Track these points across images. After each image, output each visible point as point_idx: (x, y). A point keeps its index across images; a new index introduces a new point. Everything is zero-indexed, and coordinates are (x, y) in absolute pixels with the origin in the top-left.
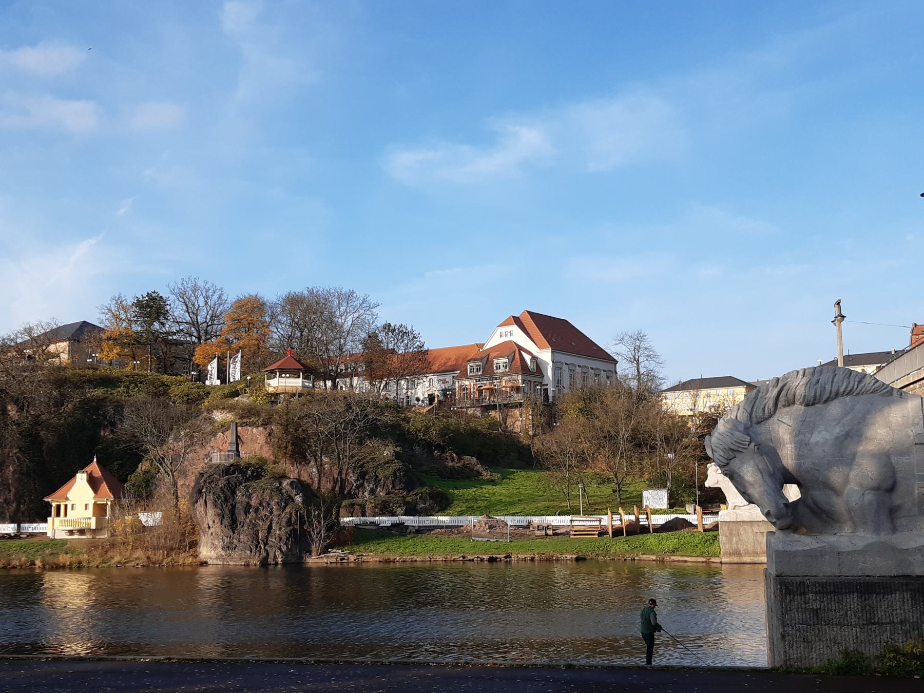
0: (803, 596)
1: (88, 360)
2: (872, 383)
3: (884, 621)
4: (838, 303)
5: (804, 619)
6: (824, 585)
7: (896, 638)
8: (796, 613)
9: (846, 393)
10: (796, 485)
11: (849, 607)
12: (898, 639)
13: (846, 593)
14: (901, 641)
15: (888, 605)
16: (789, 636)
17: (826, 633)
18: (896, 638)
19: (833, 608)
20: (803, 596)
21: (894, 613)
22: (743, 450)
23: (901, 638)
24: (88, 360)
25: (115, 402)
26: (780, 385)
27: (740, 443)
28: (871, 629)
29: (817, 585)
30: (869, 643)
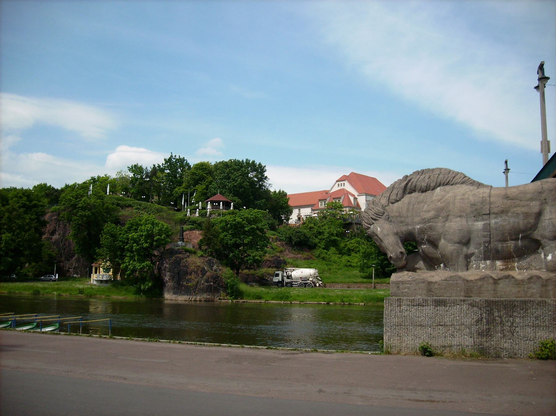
0: (399, 308)
1: (171, 203)
2: (462, 178)
3: (448, 324)
4: (506, 162)
5: (399, 322)
6: (413, 301)
7: (455, 335)
8: (394, 318)
9: (445, 184)
10: (59, 188)
11: (427, 315)
12: (456, 335)
13: (426, 306)
14: (458, 336)
15: (451, 314)
16: (389, 332)
17: (412, 331)
18: (455, 335)
19: (417, 316)
20: (399, 308)
21: (455, 319)
22: (379, 219)
23: (458, 335)
24: (171, 203)
25: (83, 209)
26: (408, 180)
27: (378, 215)
28: (440, 329)
29: (408, 301)
30: (438, 338)
